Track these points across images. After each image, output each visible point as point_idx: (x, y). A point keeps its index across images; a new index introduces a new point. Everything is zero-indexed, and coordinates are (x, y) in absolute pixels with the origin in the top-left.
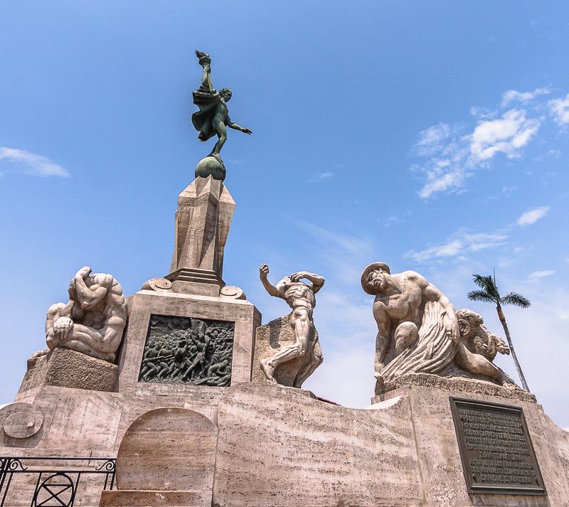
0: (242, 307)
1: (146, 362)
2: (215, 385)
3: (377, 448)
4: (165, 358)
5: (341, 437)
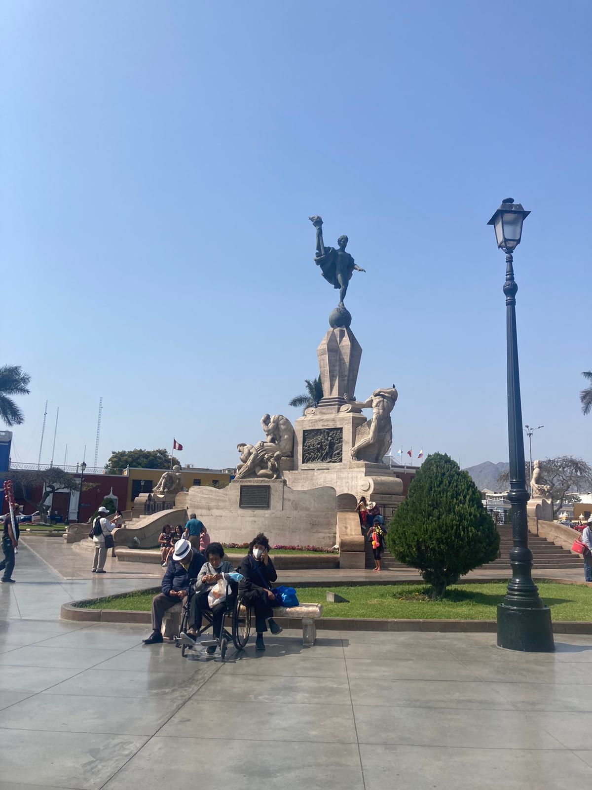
0: (346, 419)
1: (305, 454)
2: (336, 462)
3: (218, 498)
4: (313, 451)
5: (211, 496)
